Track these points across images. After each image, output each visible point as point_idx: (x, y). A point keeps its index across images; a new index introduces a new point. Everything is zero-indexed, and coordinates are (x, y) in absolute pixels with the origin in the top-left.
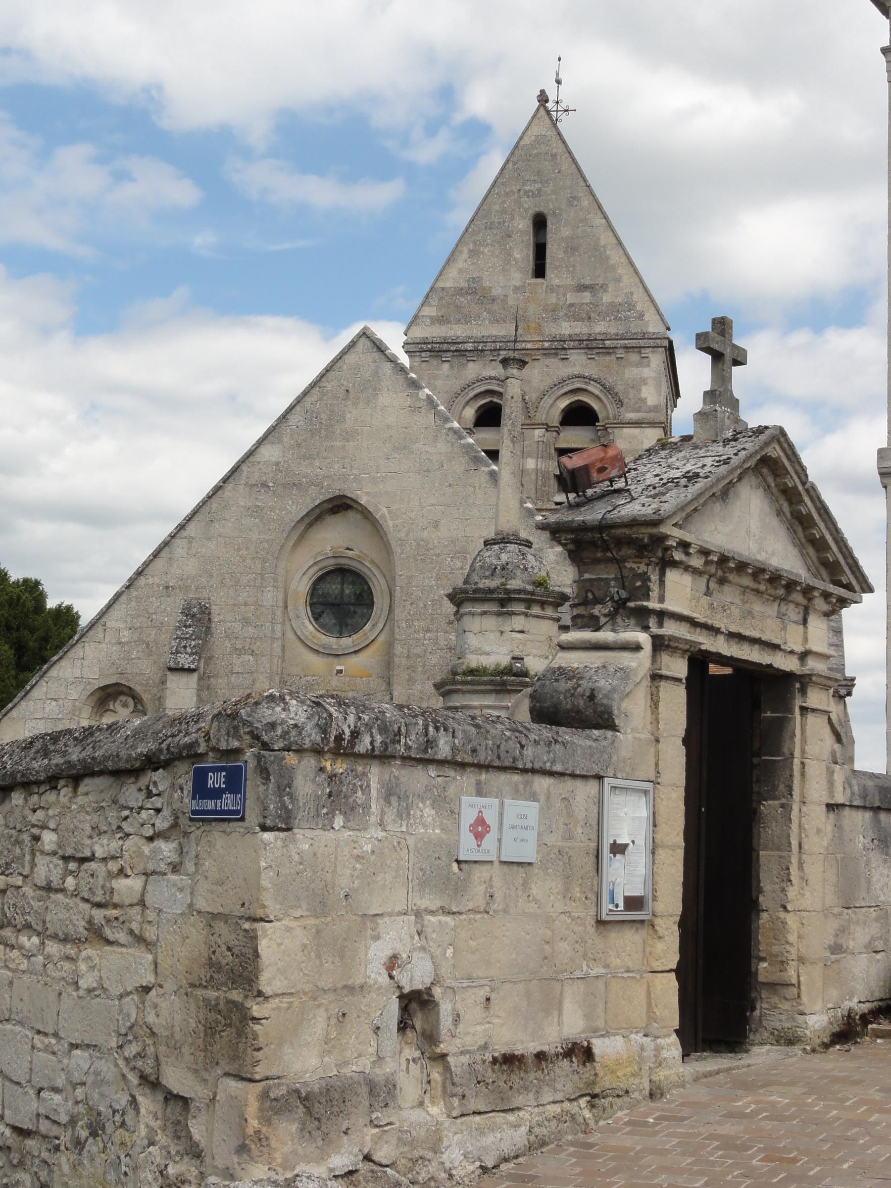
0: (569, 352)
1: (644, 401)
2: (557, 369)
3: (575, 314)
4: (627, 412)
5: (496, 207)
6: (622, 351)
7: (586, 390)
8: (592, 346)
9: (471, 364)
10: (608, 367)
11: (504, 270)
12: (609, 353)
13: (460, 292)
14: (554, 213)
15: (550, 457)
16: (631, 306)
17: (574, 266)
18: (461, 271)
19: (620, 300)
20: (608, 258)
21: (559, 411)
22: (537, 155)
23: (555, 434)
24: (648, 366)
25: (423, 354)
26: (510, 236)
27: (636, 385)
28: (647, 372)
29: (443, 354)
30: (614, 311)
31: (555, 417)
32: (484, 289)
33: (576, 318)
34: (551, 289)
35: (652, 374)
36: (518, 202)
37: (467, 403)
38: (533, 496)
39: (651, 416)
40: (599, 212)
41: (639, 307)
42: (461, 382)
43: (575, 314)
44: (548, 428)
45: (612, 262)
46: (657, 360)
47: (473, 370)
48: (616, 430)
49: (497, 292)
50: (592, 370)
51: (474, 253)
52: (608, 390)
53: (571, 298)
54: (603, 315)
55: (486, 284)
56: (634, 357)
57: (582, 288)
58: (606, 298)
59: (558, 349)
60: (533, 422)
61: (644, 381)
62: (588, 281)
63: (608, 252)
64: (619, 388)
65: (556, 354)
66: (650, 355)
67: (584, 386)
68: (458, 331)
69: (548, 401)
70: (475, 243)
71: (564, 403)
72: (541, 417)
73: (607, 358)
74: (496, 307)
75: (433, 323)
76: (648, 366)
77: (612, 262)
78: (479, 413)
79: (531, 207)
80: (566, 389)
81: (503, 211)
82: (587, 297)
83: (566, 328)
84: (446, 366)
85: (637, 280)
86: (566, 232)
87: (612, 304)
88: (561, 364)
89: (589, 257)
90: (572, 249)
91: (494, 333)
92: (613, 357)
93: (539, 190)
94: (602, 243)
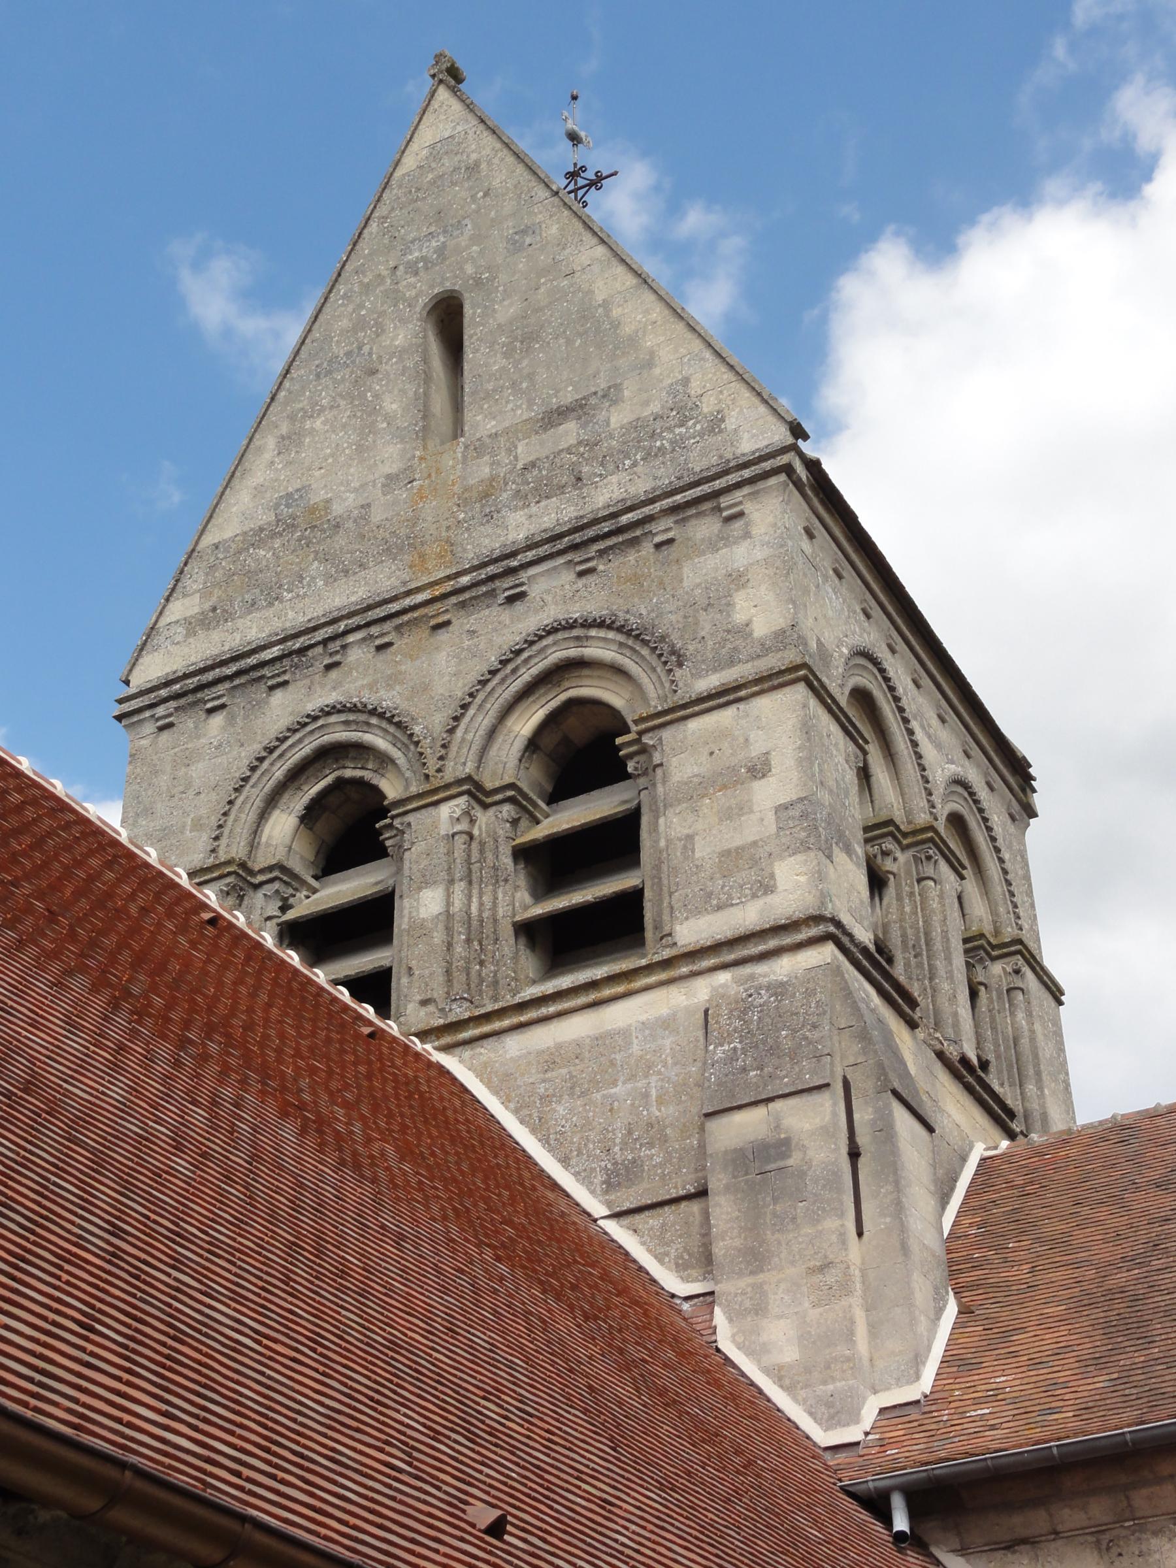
0: (524, 576)
1: (744, 631)
2: (497, 629)
3: (539, 485)
4: (697, 675)
5: (345, 323)
6: (669, 522)
7: (619, 671)
8: (585, 542)
9: (278, 696)
10: (636, 579)
11: (360, 449)
12: (634, 542)
13: (258, 537)
14: (478, 282)
15: (498, 878)
16: (682, 409)
17: (531, 377)
18: (259, 490)
19: (655, 407)
20: (616, 325)
21: (519, 745)
22: (433, 183)
23: (507, 810)
24: (747, 535)
25: (160, 711)
26: (373, 372)
27: (718, 599)
28: (741, 555)
29: (207, 694)
30: (643, 438)
31: (506, 761)
32: (312, 510)
33: (545, 491)
34: (479, 449)
35: (759, 554)
36: (394, 296)
37: (272, 801)
38: (438, 993)
39: (773, 662)
40: (588, 237)
41: (708, 406)
42: (256, 748)
43: (539, 485)
44: (476, 792)
45: (627, 330)
46: (773, 514)
47: (280, 709)
48: (667, 734)
49: (345, 504)
50: (592, 600)
51: (289, 442)
52: (633, 635)
53: (526, 451)
54: (611, 461)
55: (318, 496)
56: (704, 528)
57: (555, 417)
58: (618, 418)
59: (500, 578)
60: (436, 783)
61: (738, 579)
62: (569, 396)
63: (616, 312)
64: (670, 621)
65: (492, 594)
66: (748, 507)
67: (573, 652)
68: (252, 629)
69: (479, 721)
70: (292, 418)
71: (526, 723)
72: (460, 765)
73: (632, 557)
74: (340, 541)
75: (191, 632)
76: (747, 535)
77: (627, 330)
78: (327, 825)
79: (421, 291)
80: (526, 675)
81: (360, 324)
82: (570, 432)
83: (519, 526)
84: (218, 720)
85: (697, 345)
86: (507, 310)
87: (636, 425)
88: (506, 615)
89: (569, 342)
90: (525, 338)
91: (338, 602)
92: (647, 548)
93: (441, 251)
94: (600, 297)
